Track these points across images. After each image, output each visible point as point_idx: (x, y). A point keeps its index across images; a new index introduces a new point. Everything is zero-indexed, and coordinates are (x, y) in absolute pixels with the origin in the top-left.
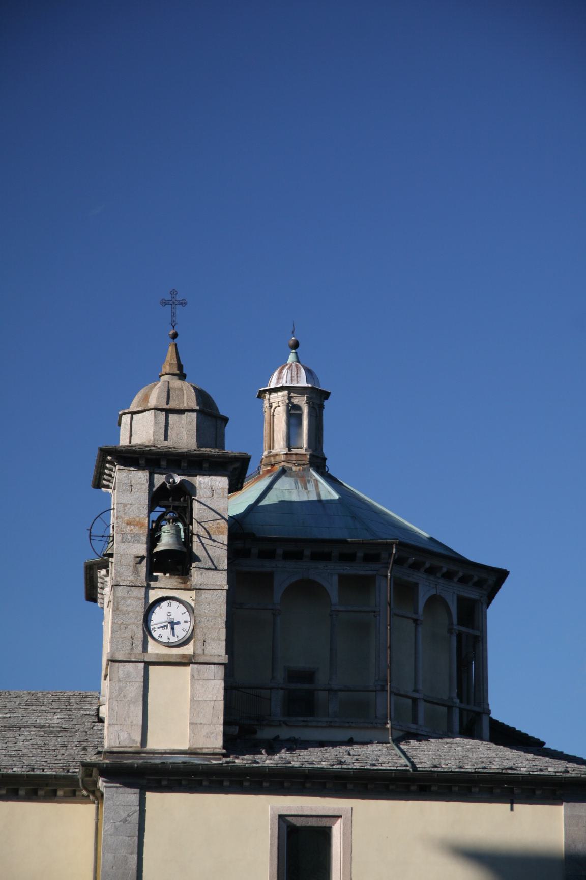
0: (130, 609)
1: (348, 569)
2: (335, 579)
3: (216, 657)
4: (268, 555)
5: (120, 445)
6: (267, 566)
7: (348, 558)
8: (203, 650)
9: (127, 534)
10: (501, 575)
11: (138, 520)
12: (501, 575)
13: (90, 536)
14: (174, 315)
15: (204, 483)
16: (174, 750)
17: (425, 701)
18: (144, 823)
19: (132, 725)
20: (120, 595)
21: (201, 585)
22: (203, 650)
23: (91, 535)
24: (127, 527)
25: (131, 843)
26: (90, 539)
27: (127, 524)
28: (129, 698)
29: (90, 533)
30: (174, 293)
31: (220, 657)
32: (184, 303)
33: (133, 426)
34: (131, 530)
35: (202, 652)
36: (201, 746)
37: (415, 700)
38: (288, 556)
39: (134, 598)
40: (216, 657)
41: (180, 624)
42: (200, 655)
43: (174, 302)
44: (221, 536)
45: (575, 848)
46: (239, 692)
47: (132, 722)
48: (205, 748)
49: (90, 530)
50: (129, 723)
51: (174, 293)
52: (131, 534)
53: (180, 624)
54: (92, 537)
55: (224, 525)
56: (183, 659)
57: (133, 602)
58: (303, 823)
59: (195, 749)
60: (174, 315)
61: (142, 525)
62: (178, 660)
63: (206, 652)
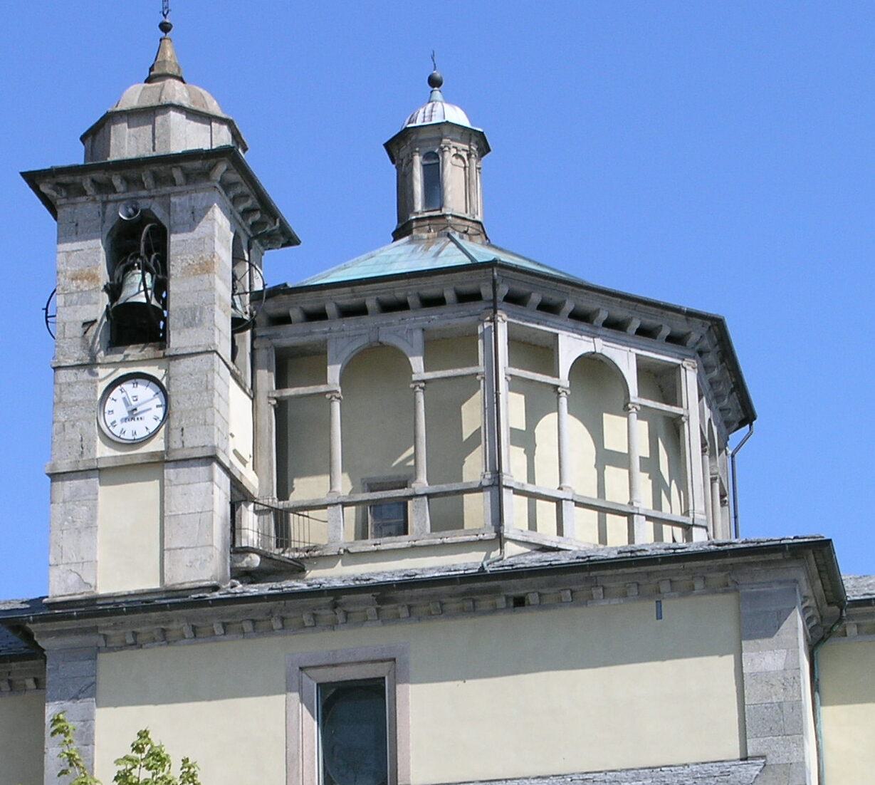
0: (79, 398)
1: (435, 319)
2: (418, 337)
3: (200, 449)
4: (317, 316)
8: (183, 442)
9: (71, 293)
11: (86, 270)
13: (47, 317)
15: (180, 205)
16: (151, 590)
17: (578, 504)
18: (582, 668)
19: (83, 563)
20: (64, 381)
21: (176, 349)
22: (183, 442)
23: (49, 315)
24: (72, 283)
25: (84, 729)
26: (47, 322)
27: (73, 279)
28: (78, 525)
29: (47, 313)
31: (204, 449)
34: (78, 287)
35: (181, 446)
36: (180, 582)
39: (83, 382)
40: (200, 449)
42: (179, 449)
44: (207, 275)
45: (161, 406)
46: (301, 517)
47: (83, 559)
48: (188, 582)
49: (46, 309)
50: (80, 560)
52: (78, 292)
54: (49, 319)
55: (147, 207)
56: (151, 458)
57: (81, 388)
58: (341, 677)
59: (173, 585)
62: (145, 461)
63: (186, 444)
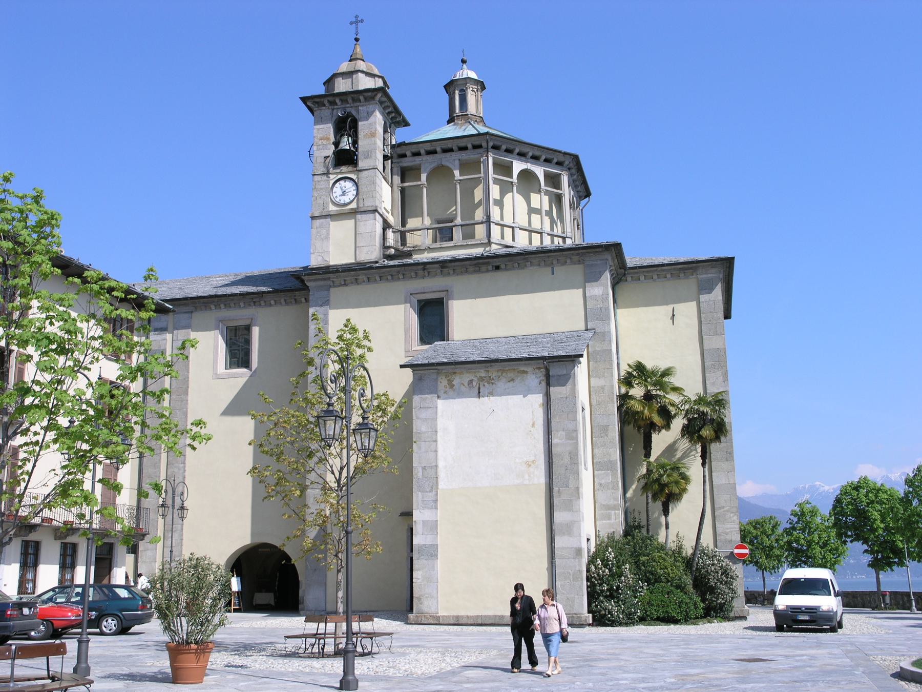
1: (464, 155)
2: (457, 162)
4: (417, 154)
5: (454, 171)
6: (418, 160)
7: (463, 149)
10: (409, 125)
12: (409, 125)
14: (357, 28)
17: (520, 229)
30: (357, 17)
32: (362, 21)
33: (756, 663)
37: (513, 228)
38: (429, 153)
41: (400, 365)
43: (357, 21)
51: (357, 17)
53: (400, 365)
60: (357, 28)
61: (307, 281)
